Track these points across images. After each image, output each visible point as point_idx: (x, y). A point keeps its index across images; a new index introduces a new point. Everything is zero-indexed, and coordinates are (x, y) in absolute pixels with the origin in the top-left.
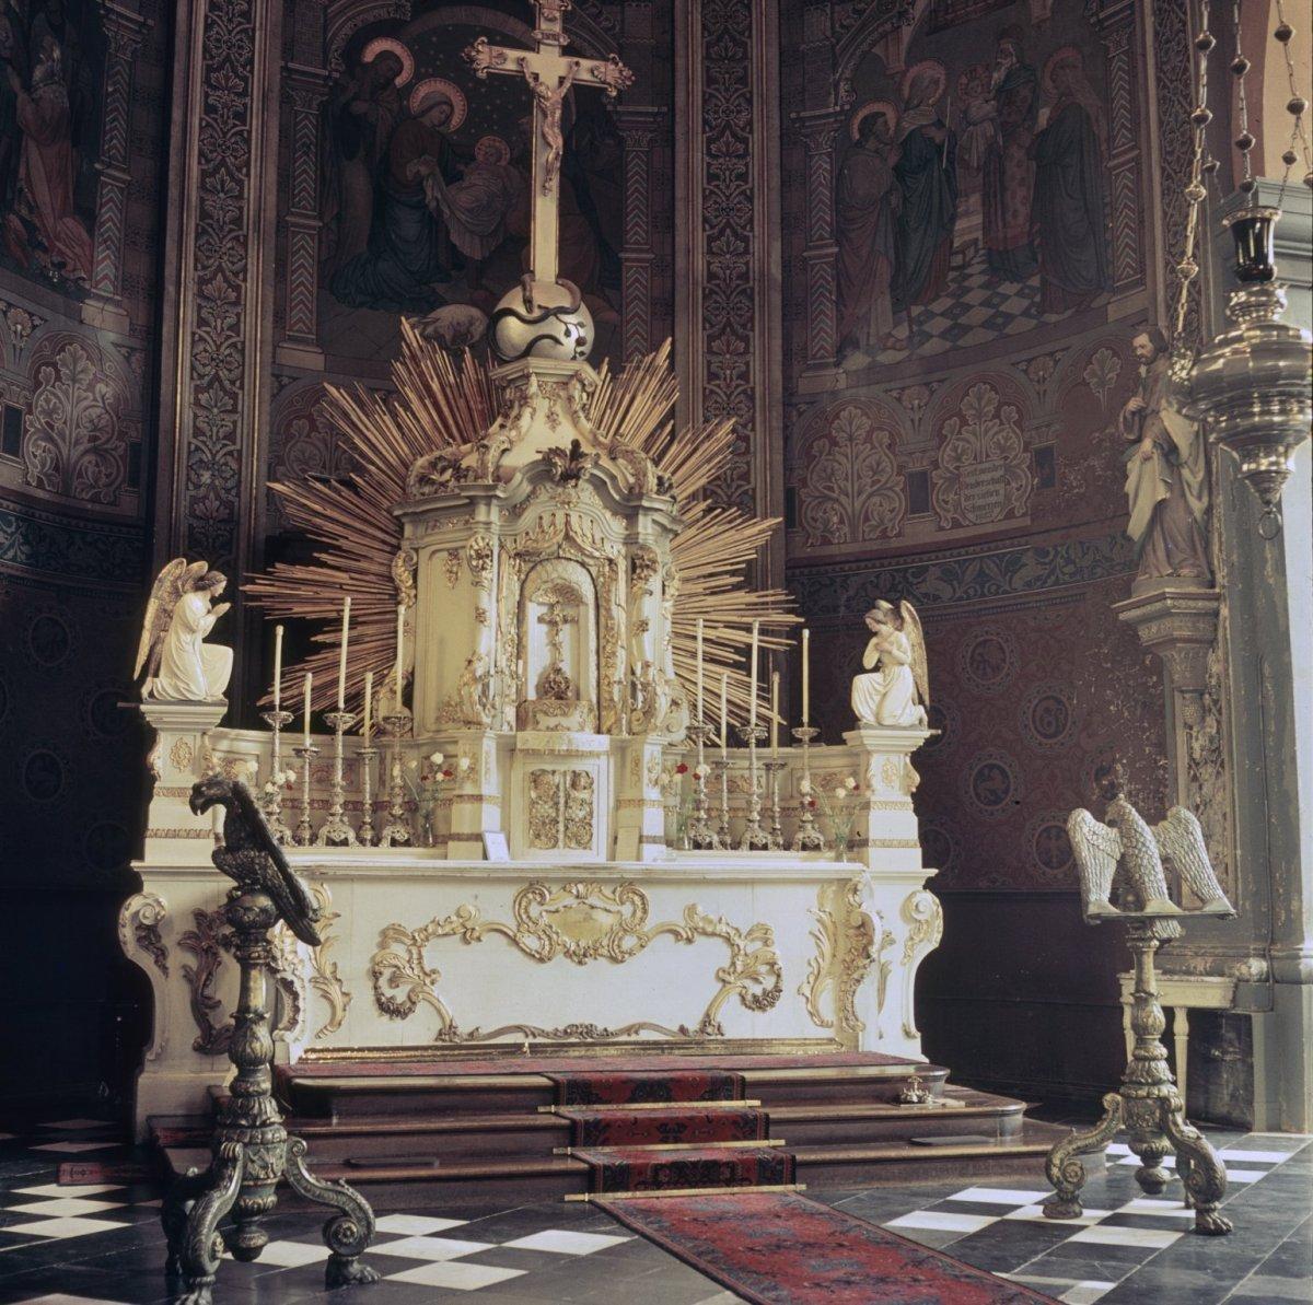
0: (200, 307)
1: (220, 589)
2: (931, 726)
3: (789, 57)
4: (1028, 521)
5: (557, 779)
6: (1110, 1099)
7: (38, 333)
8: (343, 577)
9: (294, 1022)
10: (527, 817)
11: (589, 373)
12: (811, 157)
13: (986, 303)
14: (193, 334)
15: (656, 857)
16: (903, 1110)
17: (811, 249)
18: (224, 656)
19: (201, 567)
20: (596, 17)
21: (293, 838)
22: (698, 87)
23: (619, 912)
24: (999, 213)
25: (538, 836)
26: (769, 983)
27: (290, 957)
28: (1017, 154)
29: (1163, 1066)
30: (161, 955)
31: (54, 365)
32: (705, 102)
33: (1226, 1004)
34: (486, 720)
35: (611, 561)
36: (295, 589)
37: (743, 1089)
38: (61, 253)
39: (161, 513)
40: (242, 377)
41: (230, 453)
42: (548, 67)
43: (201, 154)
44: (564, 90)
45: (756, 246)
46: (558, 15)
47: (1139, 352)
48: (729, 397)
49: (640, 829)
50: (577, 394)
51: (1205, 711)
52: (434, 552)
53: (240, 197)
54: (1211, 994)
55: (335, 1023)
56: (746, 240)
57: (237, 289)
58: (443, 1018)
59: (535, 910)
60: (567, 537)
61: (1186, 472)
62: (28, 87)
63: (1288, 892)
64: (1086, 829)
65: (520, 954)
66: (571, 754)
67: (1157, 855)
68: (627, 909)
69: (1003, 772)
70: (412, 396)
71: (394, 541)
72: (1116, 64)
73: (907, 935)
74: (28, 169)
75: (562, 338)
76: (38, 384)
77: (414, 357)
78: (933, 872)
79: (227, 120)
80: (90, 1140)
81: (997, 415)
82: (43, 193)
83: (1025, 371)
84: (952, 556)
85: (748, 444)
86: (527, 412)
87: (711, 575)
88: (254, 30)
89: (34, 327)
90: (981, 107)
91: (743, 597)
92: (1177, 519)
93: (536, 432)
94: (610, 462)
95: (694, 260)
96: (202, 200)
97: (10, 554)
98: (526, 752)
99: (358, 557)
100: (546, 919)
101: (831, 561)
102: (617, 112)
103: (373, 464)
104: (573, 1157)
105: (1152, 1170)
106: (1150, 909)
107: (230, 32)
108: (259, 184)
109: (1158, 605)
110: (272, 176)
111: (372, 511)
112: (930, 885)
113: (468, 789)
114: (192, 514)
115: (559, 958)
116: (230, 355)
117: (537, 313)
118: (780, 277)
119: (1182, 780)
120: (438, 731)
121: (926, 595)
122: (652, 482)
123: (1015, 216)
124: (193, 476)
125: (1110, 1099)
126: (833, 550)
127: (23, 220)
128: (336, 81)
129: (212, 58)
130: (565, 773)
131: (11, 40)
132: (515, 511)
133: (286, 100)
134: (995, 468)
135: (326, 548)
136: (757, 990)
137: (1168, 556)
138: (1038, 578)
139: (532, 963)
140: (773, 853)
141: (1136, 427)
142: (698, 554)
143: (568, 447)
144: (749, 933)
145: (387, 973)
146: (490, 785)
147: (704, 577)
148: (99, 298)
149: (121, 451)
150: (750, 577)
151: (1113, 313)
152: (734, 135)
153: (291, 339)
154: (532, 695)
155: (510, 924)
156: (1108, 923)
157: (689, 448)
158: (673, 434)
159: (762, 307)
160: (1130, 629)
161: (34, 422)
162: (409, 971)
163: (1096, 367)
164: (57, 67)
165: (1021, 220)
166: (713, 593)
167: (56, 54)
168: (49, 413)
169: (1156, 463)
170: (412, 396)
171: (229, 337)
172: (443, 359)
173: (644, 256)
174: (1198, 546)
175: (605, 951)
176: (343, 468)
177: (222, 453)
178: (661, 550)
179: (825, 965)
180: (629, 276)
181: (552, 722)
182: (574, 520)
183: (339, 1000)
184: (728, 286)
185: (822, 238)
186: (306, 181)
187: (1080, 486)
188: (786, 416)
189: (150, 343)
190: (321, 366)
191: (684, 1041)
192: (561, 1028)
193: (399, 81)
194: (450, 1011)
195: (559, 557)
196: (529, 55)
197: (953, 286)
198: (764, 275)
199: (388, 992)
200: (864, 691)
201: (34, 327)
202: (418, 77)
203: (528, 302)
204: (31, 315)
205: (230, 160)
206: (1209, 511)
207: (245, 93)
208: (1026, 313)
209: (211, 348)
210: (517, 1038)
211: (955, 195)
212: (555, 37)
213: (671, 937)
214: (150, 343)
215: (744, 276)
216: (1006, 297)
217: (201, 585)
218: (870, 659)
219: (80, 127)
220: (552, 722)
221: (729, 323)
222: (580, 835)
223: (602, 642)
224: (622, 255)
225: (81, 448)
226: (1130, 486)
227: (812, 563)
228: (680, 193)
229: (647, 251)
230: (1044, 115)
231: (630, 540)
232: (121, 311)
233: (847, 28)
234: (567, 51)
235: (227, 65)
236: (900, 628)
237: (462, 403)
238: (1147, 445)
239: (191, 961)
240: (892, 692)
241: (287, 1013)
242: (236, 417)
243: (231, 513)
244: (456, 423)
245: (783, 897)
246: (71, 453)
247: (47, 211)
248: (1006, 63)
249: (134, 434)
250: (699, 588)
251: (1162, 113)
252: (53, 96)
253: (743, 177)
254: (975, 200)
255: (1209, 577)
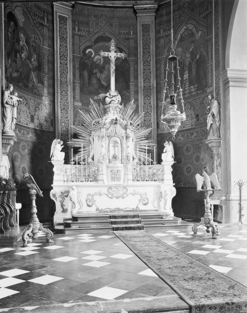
0: (61, 97)
1: (62, 144)
2: (174, 161)
3: (157, 47)
4: (195, 127)
5: (115, 171)
6: (202, 218)
7: (35, 103)
8: (83, 140)
9: (75, 208)
10: (110, 177)
11: (120, 106)
12: (161, 65)
13: (189, 90)
14: (60, 101)
15: (131, 182)
16: (163, 220)
17: (161, 81)
18: (63, 154)
19: (59, 140)
20: (124, 42)
21: (76, 181)
22: (142, 54)
23: (123, 191)
24: (191, 74)
25: (112, 180)
26: (147, 201)
27: (74, 198)
28: (194, 63)
29: (210, 213)
30: (56, 198)
31: (38, 108)
32: (143, 56)
33: (219, 204)
34: (104, 162)
35: (123, 137)
36: (73, 143)
37: (138, 216)
38: (38, 89)
39: (57, 131)
40: (68, 108)
41: (67, 120)
42: (113, 55)
43: (60, 71)
44: (115, 59)
45: (152, 81)
46: (114, 46)
47: (209, 98)
48: (147, 107)
49: (128, 178)
50: (118, 110)
51: (218, 158)
52: (96, 136)
53: (67, 78)
54: (217, 202)
55: (81, 208)
56: (150, 80)
57: (67, 93)
58: (97, 207)
59: (110, 191)
60: (116, 133)
61: (216, 119)
62: (31, 62)
63: (229, 186)
64: (198, 176)
65: (108, 197)
66: (116, 167)
67: (210, 181)
68: (124, 191)
69: (190, 168)
70: (92, 111)
71: (90, 134)
72: (209, 47)
73: (170, 194)
74: (32, 76)
75: (115, 100)
76: (36, 111)
77: (92, 104)
78: (175, 184)
79: (64, 65)
80: (49, 225)
81: (190, 109)
82: (35, 80)
83: (195, 101)
84: (183, 133)
85: (151, 115)
86: (110, 113)
87: (141, 138)
88: (67, 49)
89: (35, 102)
90: (188, 55)
91: (146, 141)
92: (214, 126)
93: (111, 116)
94: (123, 121)
95: (141, 83)
96: (61, 79)
97: (33, 138)
98: (110, 167)
99: (85, 137)
100: (112, 192)
101: (164, 134)
102: (129, 59)
103: (87, 122)
104: (112, 226)
105: (209, 229)
106: (208, 189)
107: (64, 50)
108: (70, 76)
109: (211, 141)
110: (72, 74)
111: (87, 130)
112: (174, 186)
113: (101, 173)
114: (61, 130)
115: (114, 198)
116: (66, 104)
117: (111, 96)
118: (156, 86)
119: (215, 168)
120: (97, 164)
121: (179, 139)
122: (129, 124)
123: (193, 74)
124: (61, 124)
125: (202, 218)
126: (164, 132)
127: (31, 84)
128: (82, 57)
129: (61, 55)
130: (116, 170)
131: (27, 55)
132: (108, 129)
133: (73, 61)
134: (190, 118)
135: (80, 136)
136: (145, 202)
137: (213, 133)
138: (196, 136)
139: (110, 199)
140: (150, 181)
141: (209, 111)
142: (138, 135)
143: (115, 119)
144: (143, 194)
145: (88, 201)
146: (105, 171)
147: (140, 138)
148: (45, 96)
149: (50, 121)
150: (148, 138)
151: (208, 91)
152: (148, 62)
153: (76, 101)
154: (111, 158)
155: (107, 193)
156: (201, 192)
157: (137, 117)
158: (134, 115)
159: (153, 91)
160: (207, 145)
161: (36, 117)
162: (92, 200)
163: (205, 100)
164: (36, 58)
165: (194, 75)
166: (141, 141)
167: (35, 56)
168: (38, 115)
169: (211, 117)
170: (92, 111)
171: (66, 101)
172: (97, 105)
173: (133, 84)
174: (218, 131)
175: (121, 197)
176: (83, 124)
177: (65, 120)
178: (131, 135)
179: (155, 199)
180: (131, 87)
181: (114, 162)
182: (117, 130)
183: (81, 205)
184: (147, 88)
185: (163, 79)
186: (77, 75)
187: (203, 121)
188: (157, 110)
189: (53, 103)
190: (81, 105)
191: (133, 210)
192: (115, 208)
193: (92, 56)
194: (98, 206)
195: (114, 136)
196: (109, 53)
197: (184, 87)
198: (153, 86)
199: (88, 203)
200: (164, 156)
201: (35, 102)
202: (95, 55)
203: (110, 95)
204: (34, 100)
205: (65, 72)
206: (220, 125)
207: (67, 60)
208: (195, 91)
209: (63, 103)
210: (108, 210)
211: (184, 71)
212: (113, 50)
213: (131, 195)
214: (53, 103)
215: (150, 86)
216: (192, 89)
217: (59, 143)
218: (164, 151)
219: (39, 68)
220: (114, 162)
221: (147, 95)
222: (119, 179)
223: (122, 149)
224: (130, 84)
225: (43, 121)
226: (207, 121)
227: (161, 134)
228: (139, 73)
229: (134, 83)
230: (198, 56)
231: (126, 133)
232: (49, 98)
233: (167, 42)
234: (116, 52)
235: (63, 56)
236: (169, 146)
237: (100, 111)
238: (210, 114)
239: (61, 199)
240: (168, 156)
241: (74, 207)
242: (67, 114)
243: (68, 130)
244: (99, 115)
245: (149, 189)
246: (43, 121)
247: (35, 83)
248: (192, 47)
249: (52, 118)
250: (139, 140)
251: (215, 56)
252: (35, 63)
253: (149, 69)
254: (187, 72)
255: (219, 136)
